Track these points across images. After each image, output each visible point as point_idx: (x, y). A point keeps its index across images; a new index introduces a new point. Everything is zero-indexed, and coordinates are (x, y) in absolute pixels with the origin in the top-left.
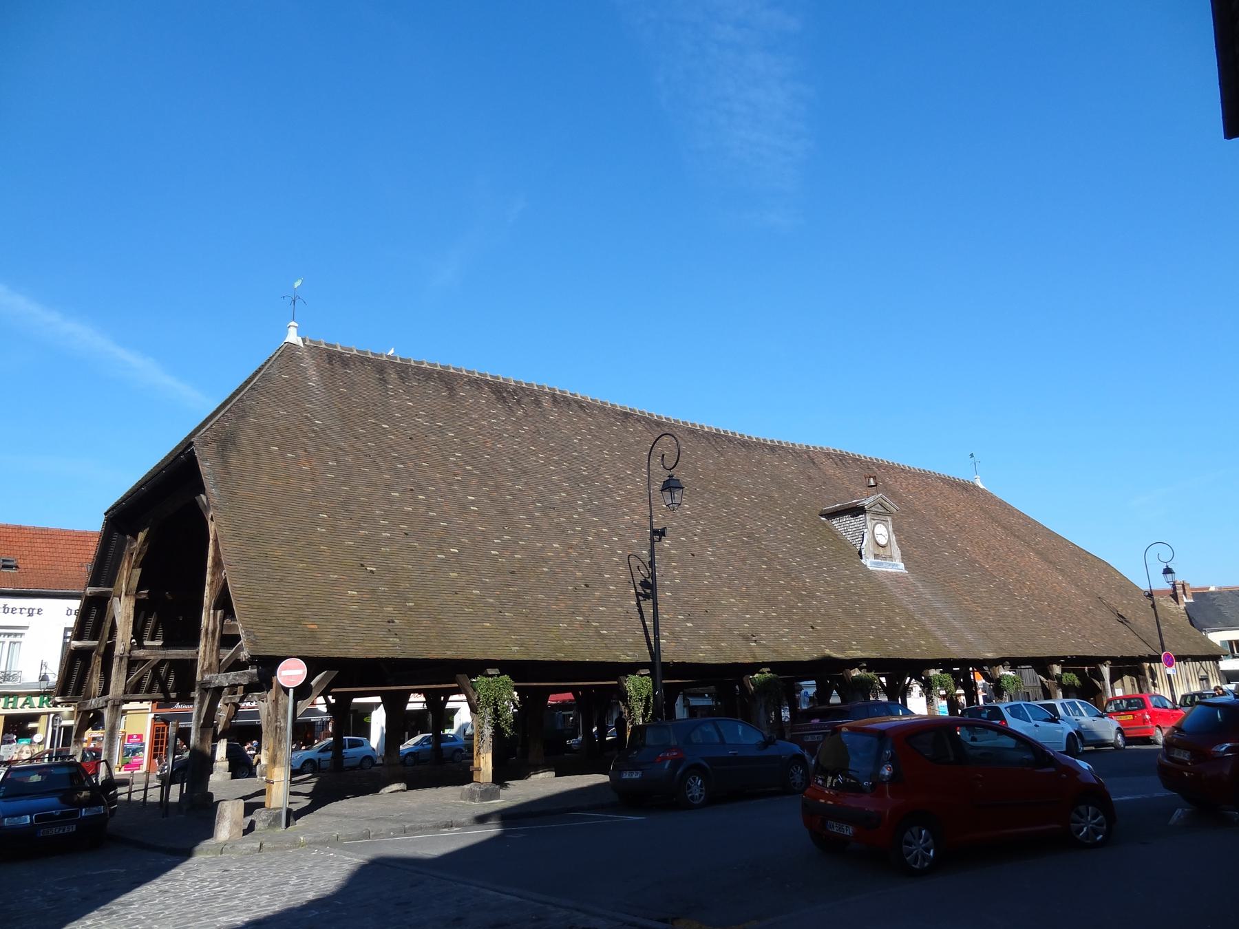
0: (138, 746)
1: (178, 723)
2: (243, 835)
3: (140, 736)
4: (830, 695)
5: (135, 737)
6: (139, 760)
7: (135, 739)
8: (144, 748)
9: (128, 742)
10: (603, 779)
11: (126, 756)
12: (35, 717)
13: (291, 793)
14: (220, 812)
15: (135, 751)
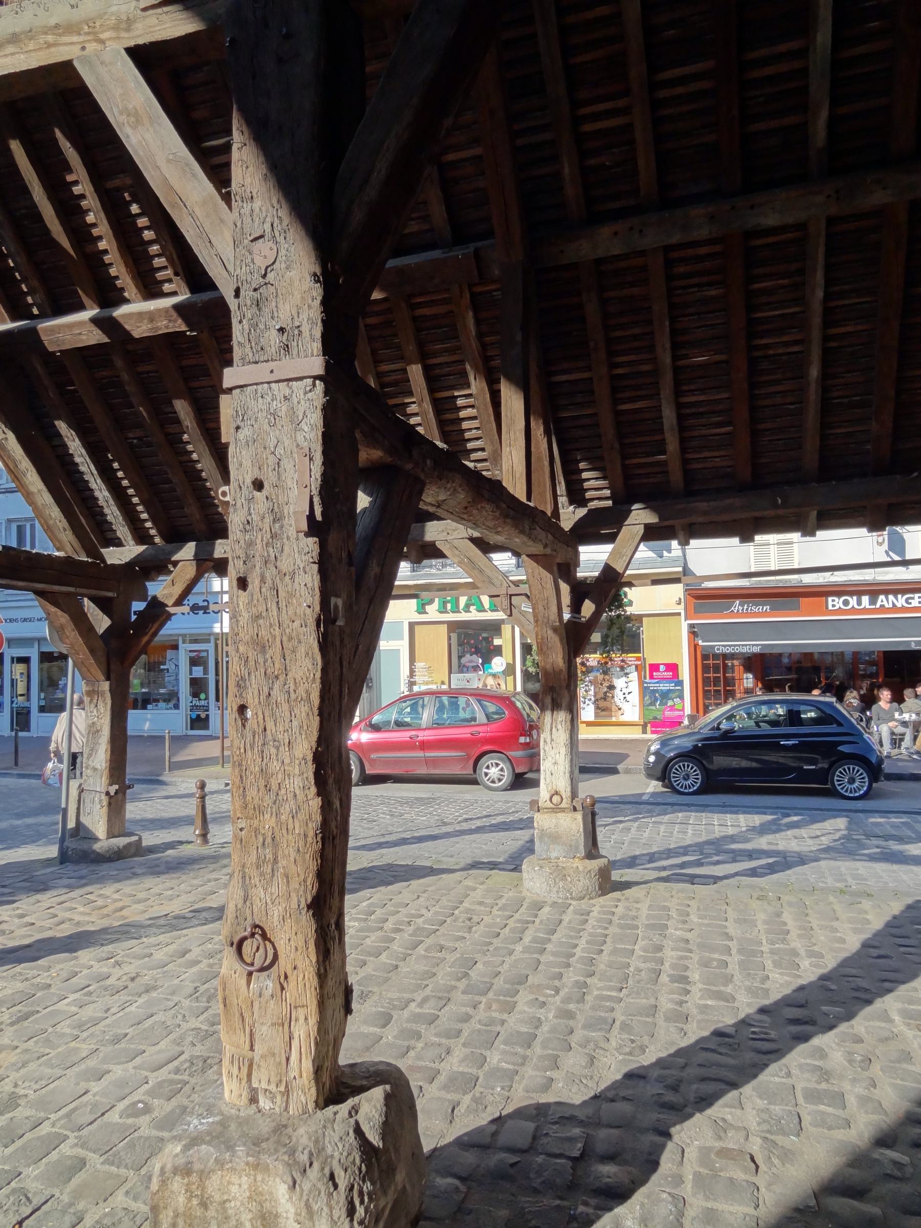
0: (671, 686)
1: (226, 592)
2: (439, 554)
3: (673, 668)
4: (356, 452)
5: (662, 668)
6: (677, 713)
7: (663, 672)
8: (682, 691)
9: (652, 677)
10: (58, 134)
11: (651, 704)
12: (495, 628)
13: (667, 472)
14: (194, 175)
15: (665, 695)
